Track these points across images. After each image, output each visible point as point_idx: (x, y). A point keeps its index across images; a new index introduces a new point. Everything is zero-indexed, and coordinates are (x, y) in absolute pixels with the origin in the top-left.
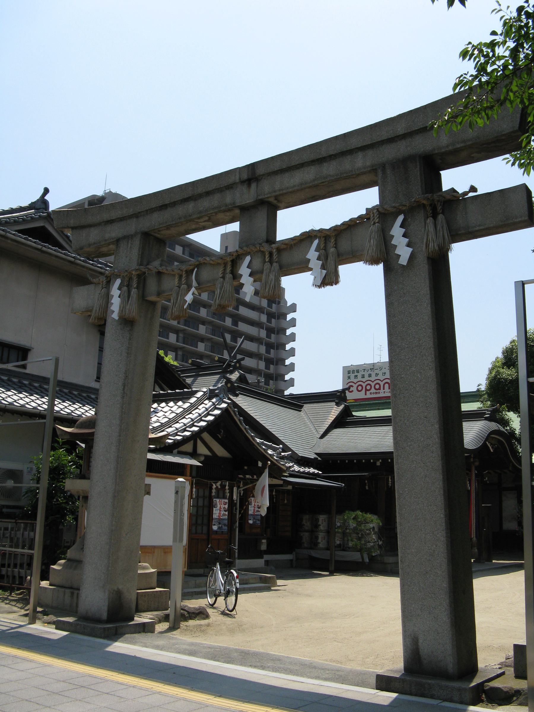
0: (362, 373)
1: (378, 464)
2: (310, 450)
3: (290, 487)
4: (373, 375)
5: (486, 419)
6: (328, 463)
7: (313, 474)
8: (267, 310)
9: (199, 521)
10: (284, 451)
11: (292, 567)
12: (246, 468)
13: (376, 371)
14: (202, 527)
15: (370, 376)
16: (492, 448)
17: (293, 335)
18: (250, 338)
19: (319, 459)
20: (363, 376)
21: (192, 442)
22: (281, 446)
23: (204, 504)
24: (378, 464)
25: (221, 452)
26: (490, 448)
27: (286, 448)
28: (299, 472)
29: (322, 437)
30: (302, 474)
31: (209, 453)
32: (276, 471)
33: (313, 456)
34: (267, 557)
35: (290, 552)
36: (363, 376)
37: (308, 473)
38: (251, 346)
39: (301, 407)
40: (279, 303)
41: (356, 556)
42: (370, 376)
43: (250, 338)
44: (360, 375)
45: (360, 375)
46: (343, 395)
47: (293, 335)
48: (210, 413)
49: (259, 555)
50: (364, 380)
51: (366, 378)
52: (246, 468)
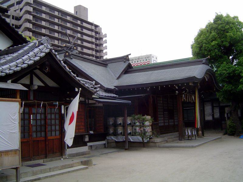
0: (135, 60)
1: (148, 90)
2: (112, 85)
3: (101, 105)
4: (139, 61)
5: (203, 63)
6: (121, 91)
7: (113, 97)
8: (95, 37)
9: (39, 129)
10: (96, 84)
11: (105, 147)
12: (68, 93)
13: (140, 60)
14: (41, 133)
15: (138, 61)
16: (207, 79)
17: (106, 53)
18: (89, 49)
19: (117, 89)
20: (135, 62)
21: (29, 76)
22: (94, 82)
23: (41, 118)
24: (148, 90)
25: (51, 83)
26: (206, 79)
27: (97, 83)
28: (105, 96)
29: (118, 78)
30: (107, 97)
31: (42, 84)
32: (86, 94)
33: (113, 88)
34: (89, 144)
35: (104, 140)
36: (135, 62)
37: (111, 97)
38: (89, 52)
39: (107, 65)
40: (99, 34)
41: (138, 139)
42: (138, 61)
43: (89, 49)
44: (134, 61)
45: (134, 61)
46: (127, 58)
47: (106, 53)
48: (37, 55)
49: (85, 144)
50: (135, 63)
51: (136, 62)
52: (68, 93)
